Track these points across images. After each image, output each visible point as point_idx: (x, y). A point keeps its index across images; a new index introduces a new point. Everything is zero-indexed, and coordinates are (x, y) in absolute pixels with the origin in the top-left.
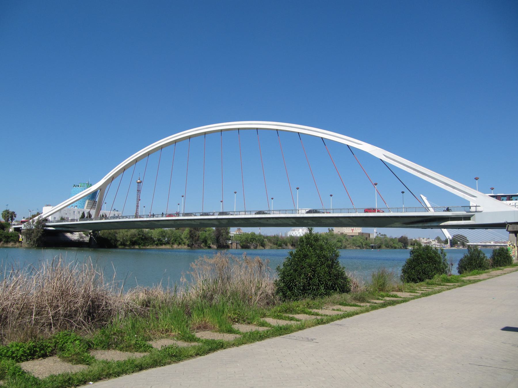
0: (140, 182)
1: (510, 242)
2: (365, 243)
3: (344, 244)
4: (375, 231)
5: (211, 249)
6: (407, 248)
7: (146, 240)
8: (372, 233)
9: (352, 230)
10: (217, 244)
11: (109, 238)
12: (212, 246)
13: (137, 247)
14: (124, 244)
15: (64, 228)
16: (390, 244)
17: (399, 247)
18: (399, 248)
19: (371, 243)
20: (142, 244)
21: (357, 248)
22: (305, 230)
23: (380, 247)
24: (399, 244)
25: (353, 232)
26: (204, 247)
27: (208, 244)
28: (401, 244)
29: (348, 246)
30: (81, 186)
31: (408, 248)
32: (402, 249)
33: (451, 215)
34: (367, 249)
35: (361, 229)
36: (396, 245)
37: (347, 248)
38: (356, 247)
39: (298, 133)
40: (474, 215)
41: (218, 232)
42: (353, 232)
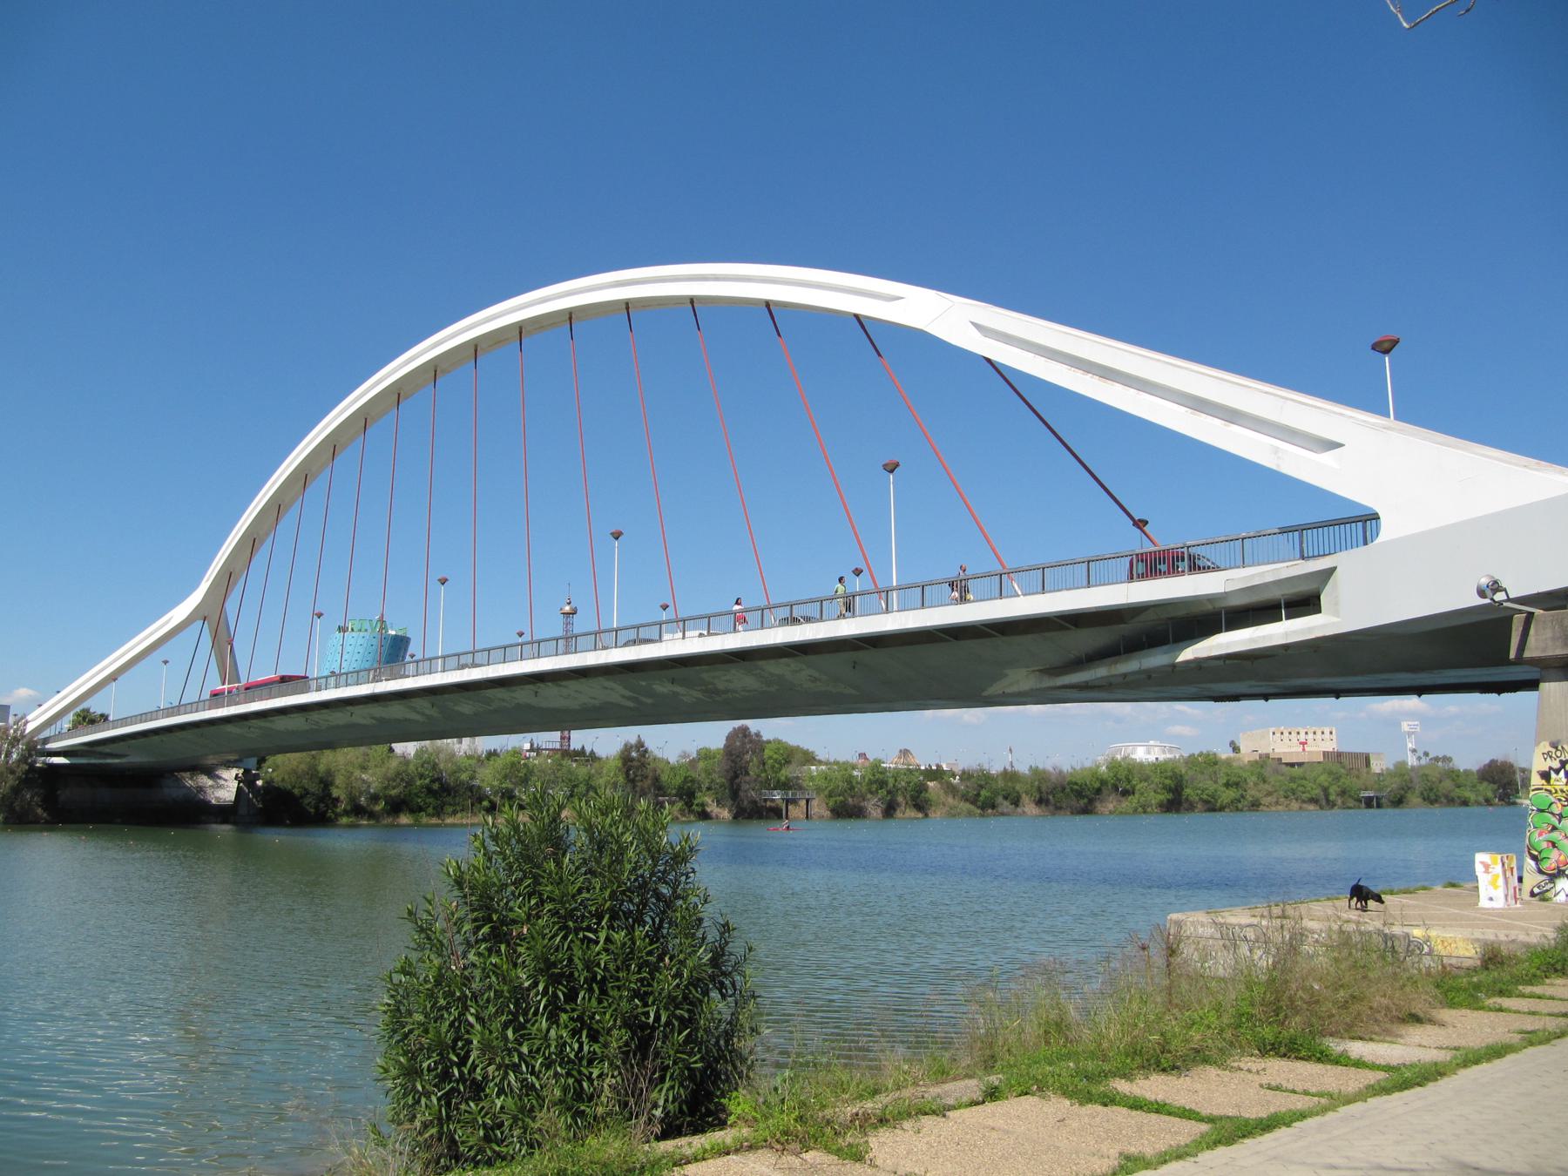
0: (574, 612)
1: (1545, 747)
2: (1339, 790)
3: (1252, 793)
4: (1410, 745)
5: (709, 821)
6: (1514, 804)
7: (449, 795)
8: (1379, 754)
9: (1301, 743)
10: (732, 802)
11: (296, 792)
12: (713, 808)
13: (405, 819)
14: (357, 810)
15: (95, 758)
16: (1440, 789)
17: (1481, 799)
18: (1478, 803)
19: (1363, 787)
20: (430, 810)
21: (1305, 805)
22: (1156, 749)
23: (1398, 802)
24: (1481, 789)
25: (1304, 750)
26: (679, 816)
27: (697, 805)
28: (1487, 789)
29: (1266, 801)
30: (352, 630)
31: (1518, 801)
32: (1336, 810)
33: (1221, 590)
34: (1350, 808)
35: (1335, 740)
36: (1468, 794)
37: (1265, 808)
38: (1304, 802)
39: (768, 304)
40: (1333, 570)
41: (730, 762)
42: (1304, 750)
